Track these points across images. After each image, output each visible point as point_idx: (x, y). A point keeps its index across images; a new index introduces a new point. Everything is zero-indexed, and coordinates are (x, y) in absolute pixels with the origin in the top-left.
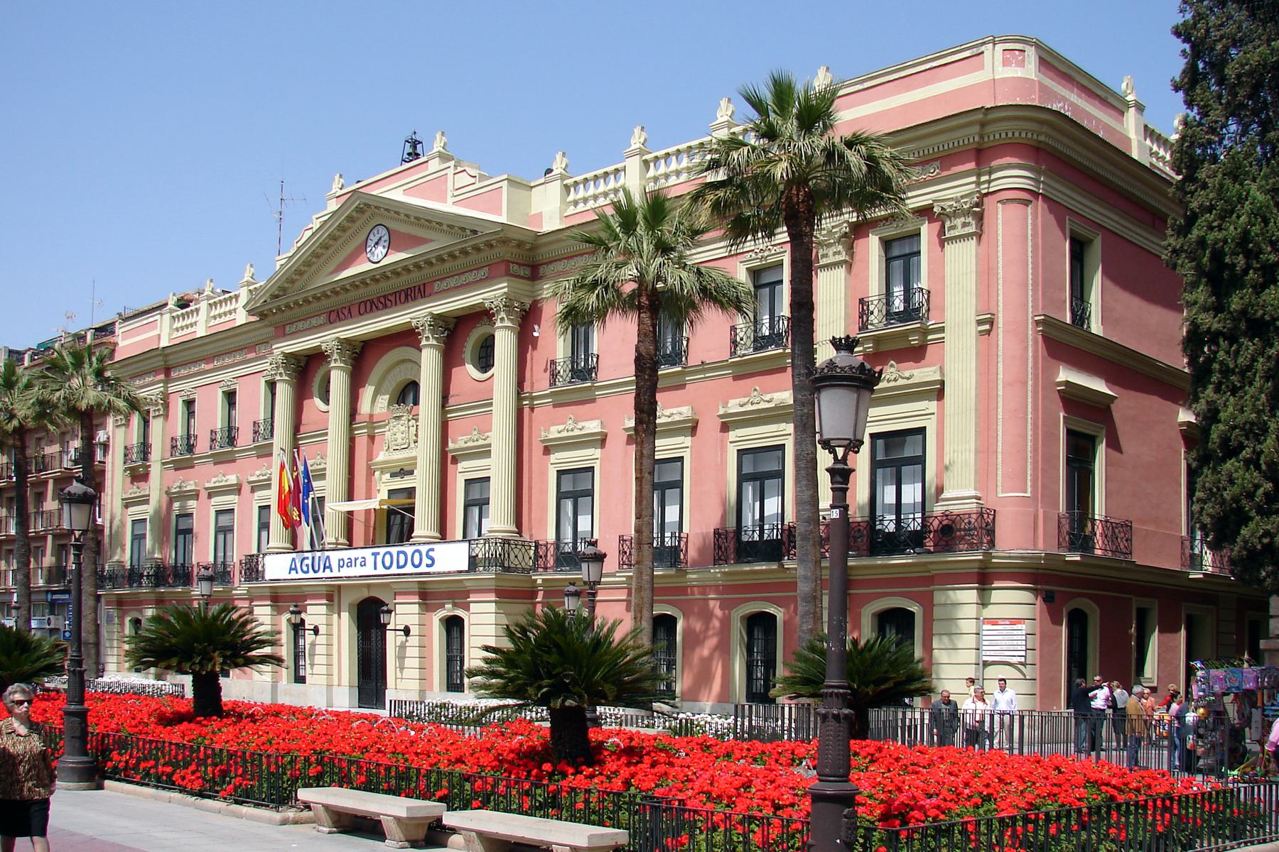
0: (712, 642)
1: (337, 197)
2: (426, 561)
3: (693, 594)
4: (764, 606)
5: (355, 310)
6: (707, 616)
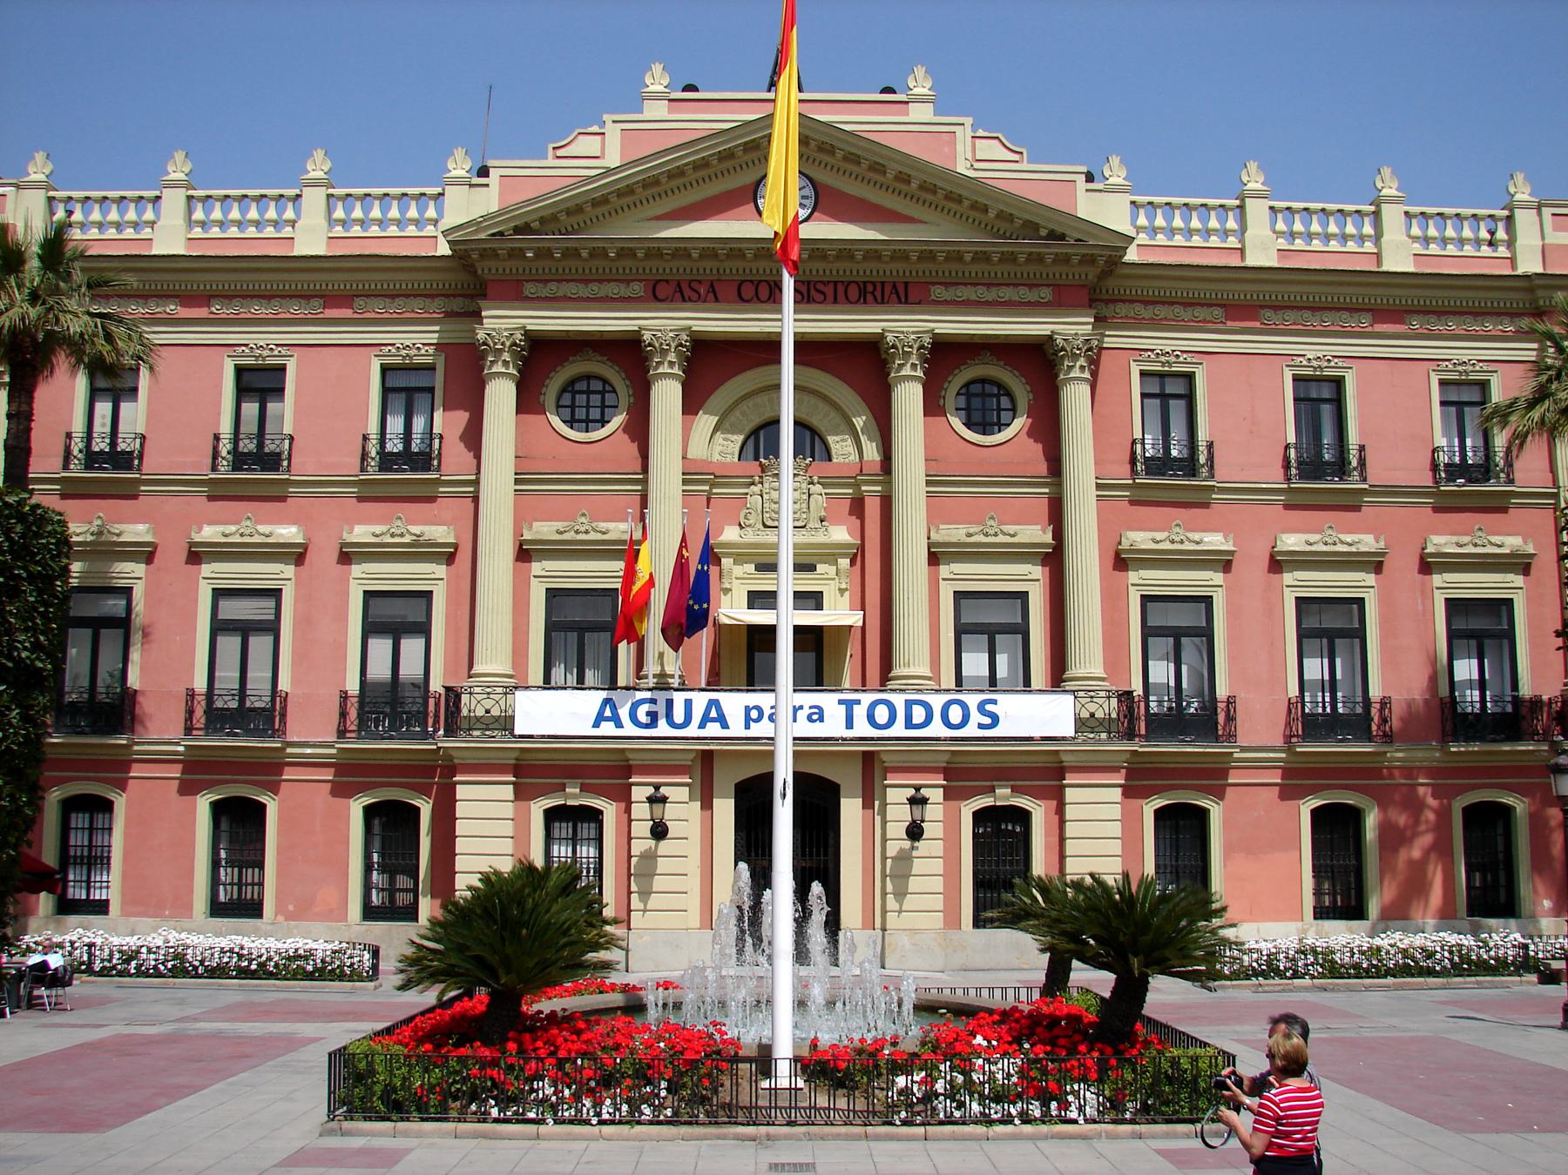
0: (1426, 840)
1: (670, 100)
2: (976, 717)
3: (1391, 776)
4: (252, 791)
5: (854, 292)
6: (1414, 806)
